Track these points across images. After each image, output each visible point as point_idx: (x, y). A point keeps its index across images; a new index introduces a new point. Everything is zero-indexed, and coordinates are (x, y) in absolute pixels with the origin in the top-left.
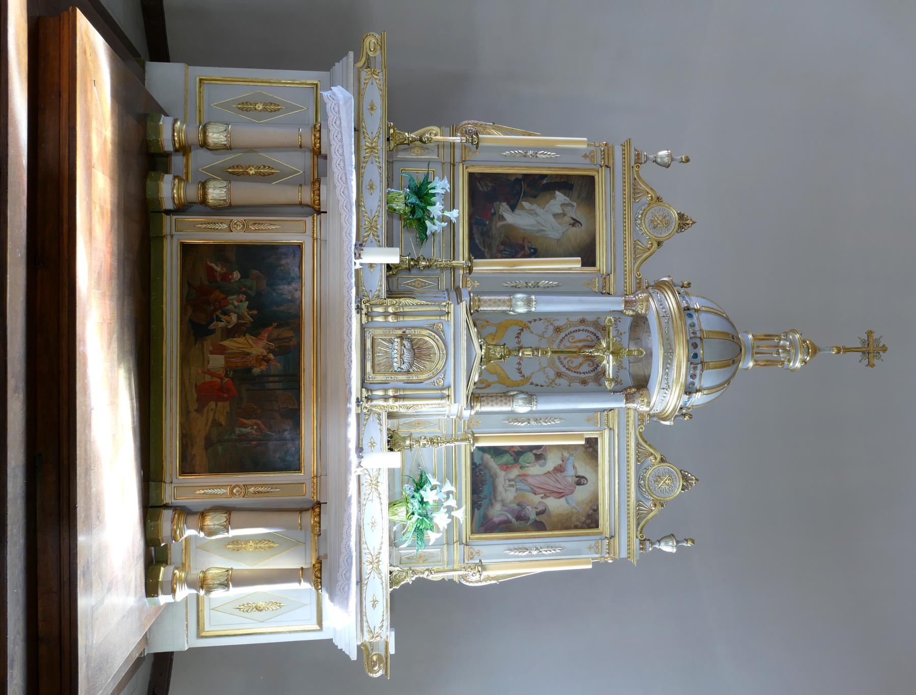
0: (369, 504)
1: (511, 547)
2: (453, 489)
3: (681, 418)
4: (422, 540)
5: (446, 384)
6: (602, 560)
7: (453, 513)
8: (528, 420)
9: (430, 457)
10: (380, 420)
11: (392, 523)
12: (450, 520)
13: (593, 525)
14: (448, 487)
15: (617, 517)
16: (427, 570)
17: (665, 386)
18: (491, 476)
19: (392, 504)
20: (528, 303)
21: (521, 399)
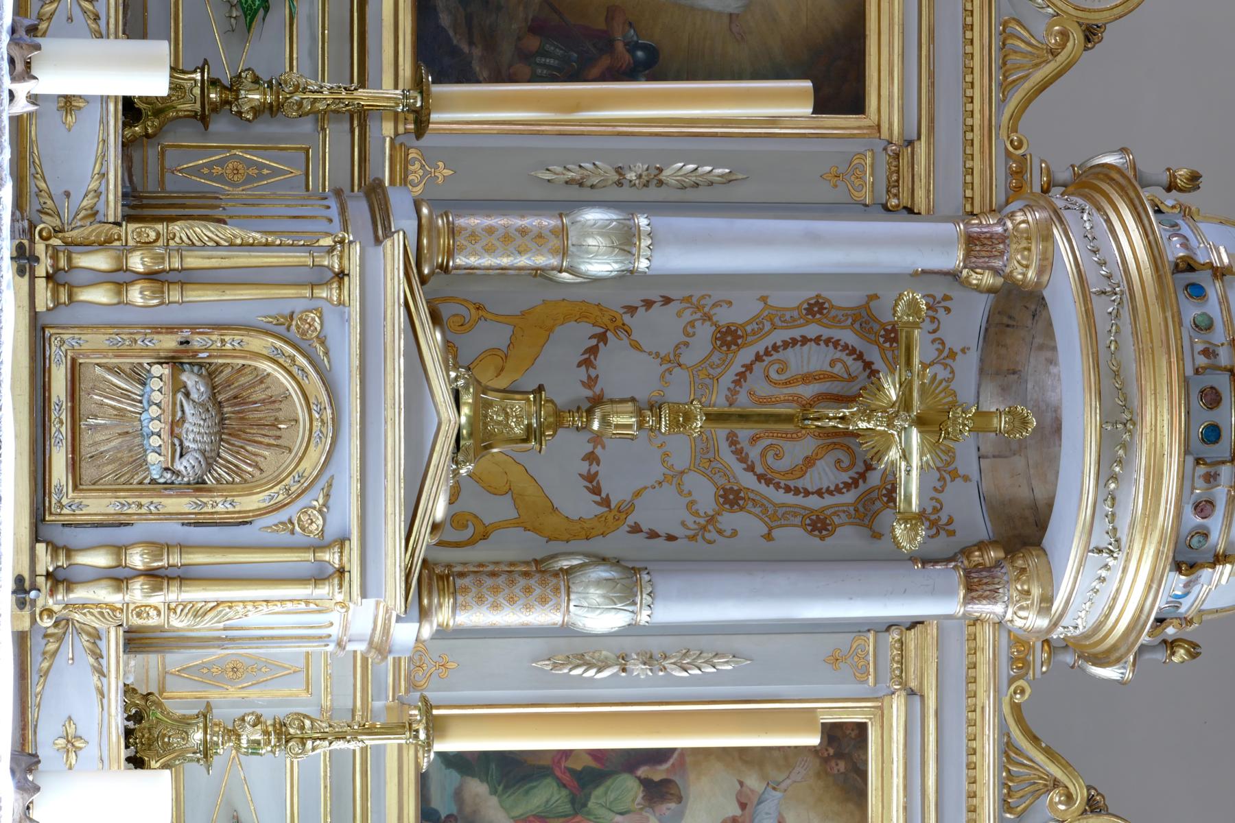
3: (1161, 656)
5: (332, 532)
8: (623, 661)
10: (98, 656)
20: (626, 240)
21: (599, 583)
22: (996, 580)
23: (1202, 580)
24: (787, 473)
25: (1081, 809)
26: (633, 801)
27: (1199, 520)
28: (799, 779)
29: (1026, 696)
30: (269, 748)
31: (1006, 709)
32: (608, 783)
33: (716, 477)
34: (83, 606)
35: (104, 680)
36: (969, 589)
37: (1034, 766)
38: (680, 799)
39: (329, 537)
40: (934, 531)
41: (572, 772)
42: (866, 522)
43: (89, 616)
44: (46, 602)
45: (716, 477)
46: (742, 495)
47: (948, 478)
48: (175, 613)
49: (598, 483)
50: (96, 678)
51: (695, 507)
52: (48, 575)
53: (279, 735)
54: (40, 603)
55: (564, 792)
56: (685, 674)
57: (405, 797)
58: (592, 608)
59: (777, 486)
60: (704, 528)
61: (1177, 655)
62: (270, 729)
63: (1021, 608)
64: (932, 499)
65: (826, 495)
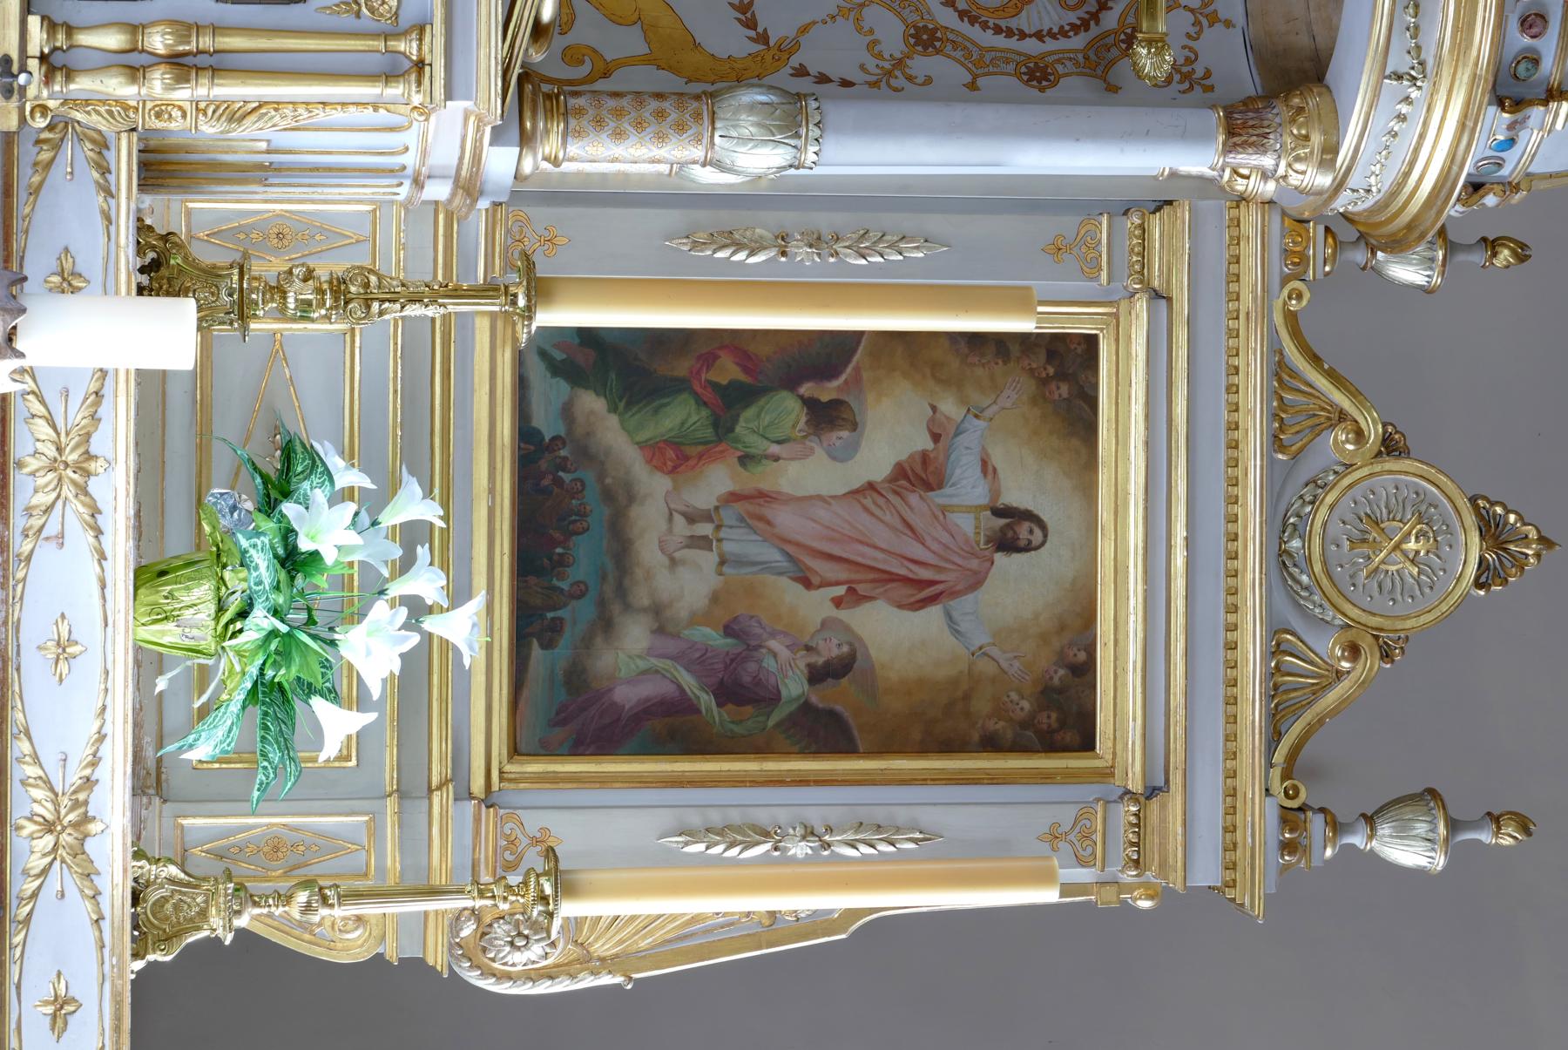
0: (46, 556)
1: (695, 819)
2: (431, 512)
3: (1479, 257)
4: (286, 746)
5: (408, 16)
6: (1109, 896)
7: (430, 624)
8: (782, 242)
9: (322, 362)
10: (105, 170)
11: (148, 662)
12: (415, 639)
13: (1069, 737)
14: (413, 505)
15: (1178, 715)
16: (307, 884)
17: (1400, 61)
18: (608, 496)
19: (149, 574)
21: (752, 108)
22: (1266, 123)
23: (1531, 122)
24: (996, 10)
25: (1376, 450)
26: (794, 427)
27: (1527, 40)
28: (1008, 405)
29: (1304, 303)
30: (323, 312)
31: (1278, 319)
32: (762, 402)
33: (906, 12)
34: (85, 103)
35: (112, 202)
36: (1231, 132)
37: (1312, 392)
38: (854, 426)
39: (405, 21)
40: (1187, 85)
41: (715, 386)
42: (1099, 72)
43: (95, 117)
44: (40, 91)
45: (906, 12)
46: (939, 34)
47: (1205, 22)
48: (205, 114)
49: (753, 14)
50: (101, 199)
51: (877, 49)
52: (43, 58)
53: (336, 294)
54: (32, 91)
55: (705, 412)
56: (863, 262)
57: (499, 410)
58: (742, 140)
59: (985, 26)
60: (889, 74)
61: (1501, 257)
62: (325, 286)
63: (1298, 159)
64: (1184, 47)
65: (1047, 39)
